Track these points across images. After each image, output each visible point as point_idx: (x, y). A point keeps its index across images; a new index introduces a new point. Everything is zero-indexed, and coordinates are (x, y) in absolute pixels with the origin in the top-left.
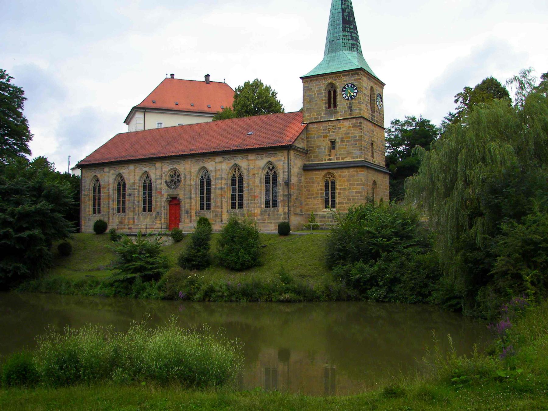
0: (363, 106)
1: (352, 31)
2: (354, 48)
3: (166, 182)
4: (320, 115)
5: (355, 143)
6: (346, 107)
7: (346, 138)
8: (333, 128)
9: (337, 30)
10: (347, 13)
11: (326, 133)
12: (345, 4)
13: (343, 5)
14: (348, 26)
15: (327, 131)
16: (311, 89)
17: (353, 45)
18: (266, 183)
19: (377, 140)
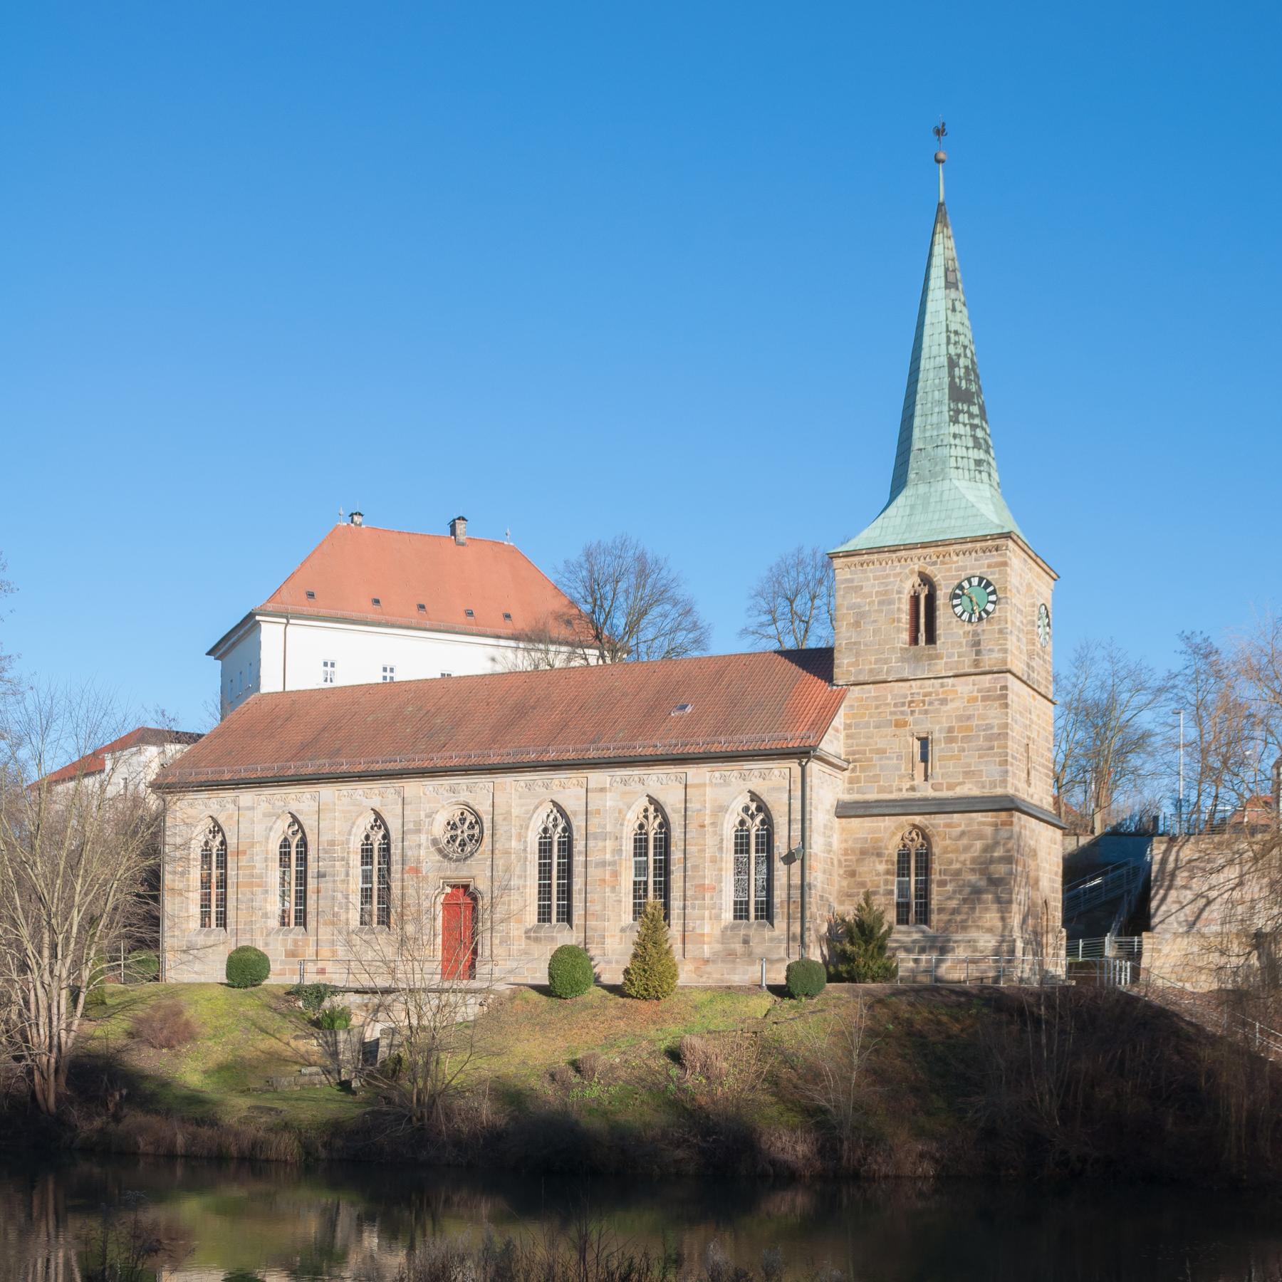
0: (1012, 643)
1: (977, 421)
2: (980, 472)
3: (435, 842)
4: (886, 661)
5: (987, 744)
6: (964, 641)
7: (961, 729)
8: (923, 702)
9: (935, 419)
10: (963, 371)
11: (902, 713)
12: (956, 343)
13: (951, 347)
14: (965, 408)
15: (906, 708)
16: (861, 587)
17: (978, 462)
18: (736, 852)
19: (1038, 736)
